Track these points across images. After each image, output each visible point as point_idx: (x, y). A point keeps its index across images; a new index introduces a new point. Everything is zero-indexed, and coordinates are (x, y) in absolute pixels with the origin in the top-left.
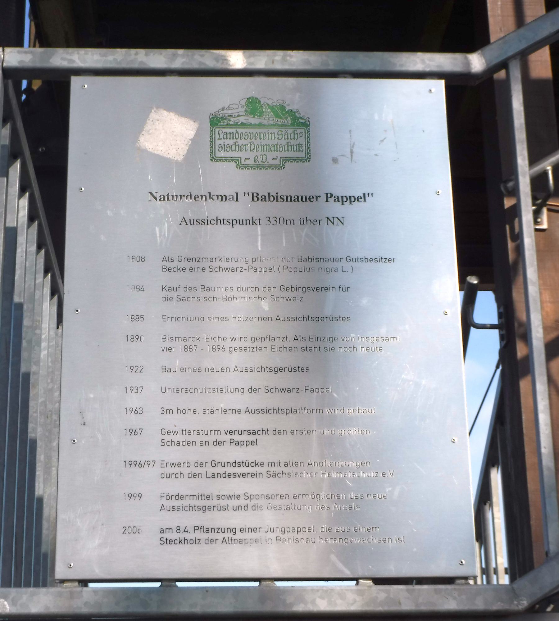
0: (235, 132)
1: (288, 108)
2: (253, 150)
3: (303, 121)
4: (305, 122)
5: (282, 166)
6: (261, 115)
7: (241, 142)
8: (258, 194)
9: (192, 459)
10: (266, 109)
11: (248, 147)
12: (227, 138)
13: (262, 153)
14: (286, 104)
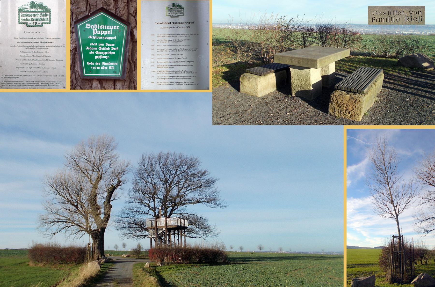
1: (44, 5)
6: (175, 7)
7: (171, 12)
9: (163, 70)
10: (37, 6)
11: (31, 20)
13: (35, 22)
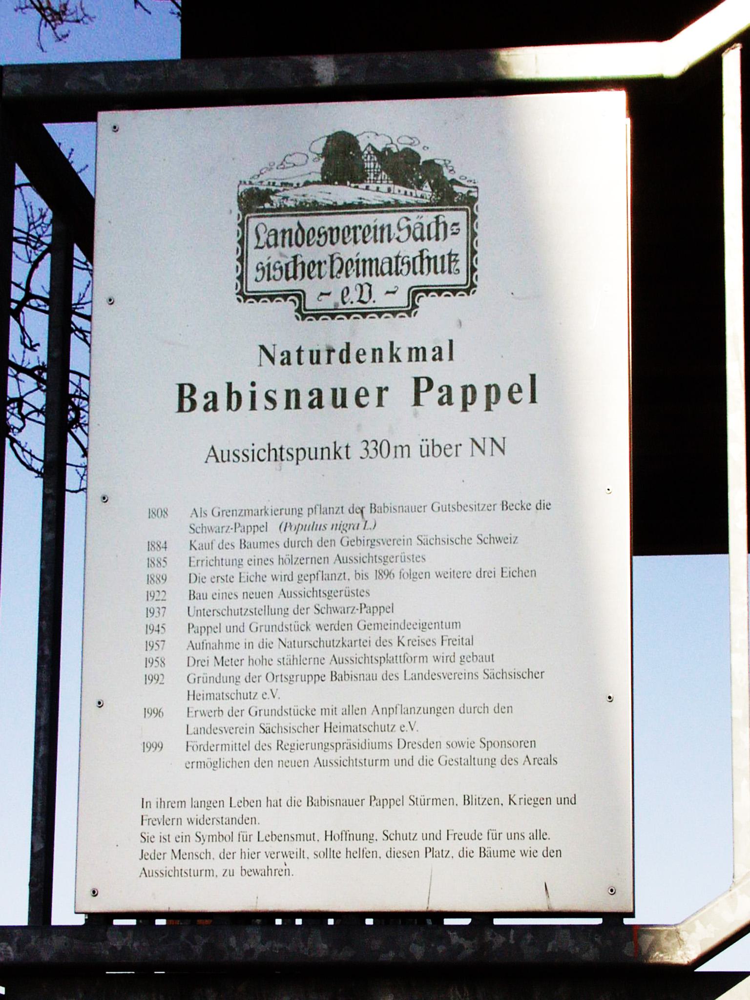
0: (295, 228)
2: (338, 275)
3: (465, 191)
4: (469, 192)
5: (412, 309)
8: (193, 390)
12: (276, 245)
14: (422, 145)
